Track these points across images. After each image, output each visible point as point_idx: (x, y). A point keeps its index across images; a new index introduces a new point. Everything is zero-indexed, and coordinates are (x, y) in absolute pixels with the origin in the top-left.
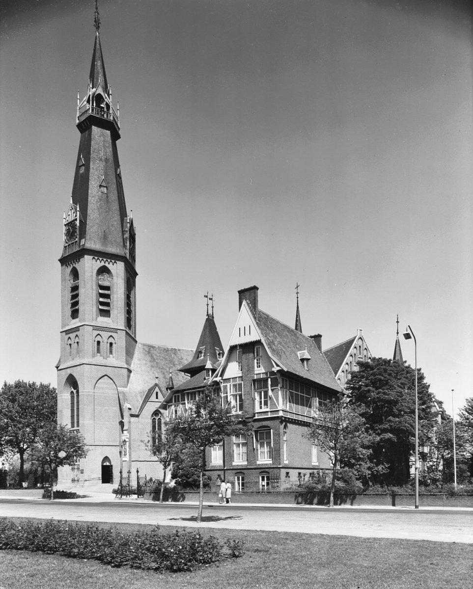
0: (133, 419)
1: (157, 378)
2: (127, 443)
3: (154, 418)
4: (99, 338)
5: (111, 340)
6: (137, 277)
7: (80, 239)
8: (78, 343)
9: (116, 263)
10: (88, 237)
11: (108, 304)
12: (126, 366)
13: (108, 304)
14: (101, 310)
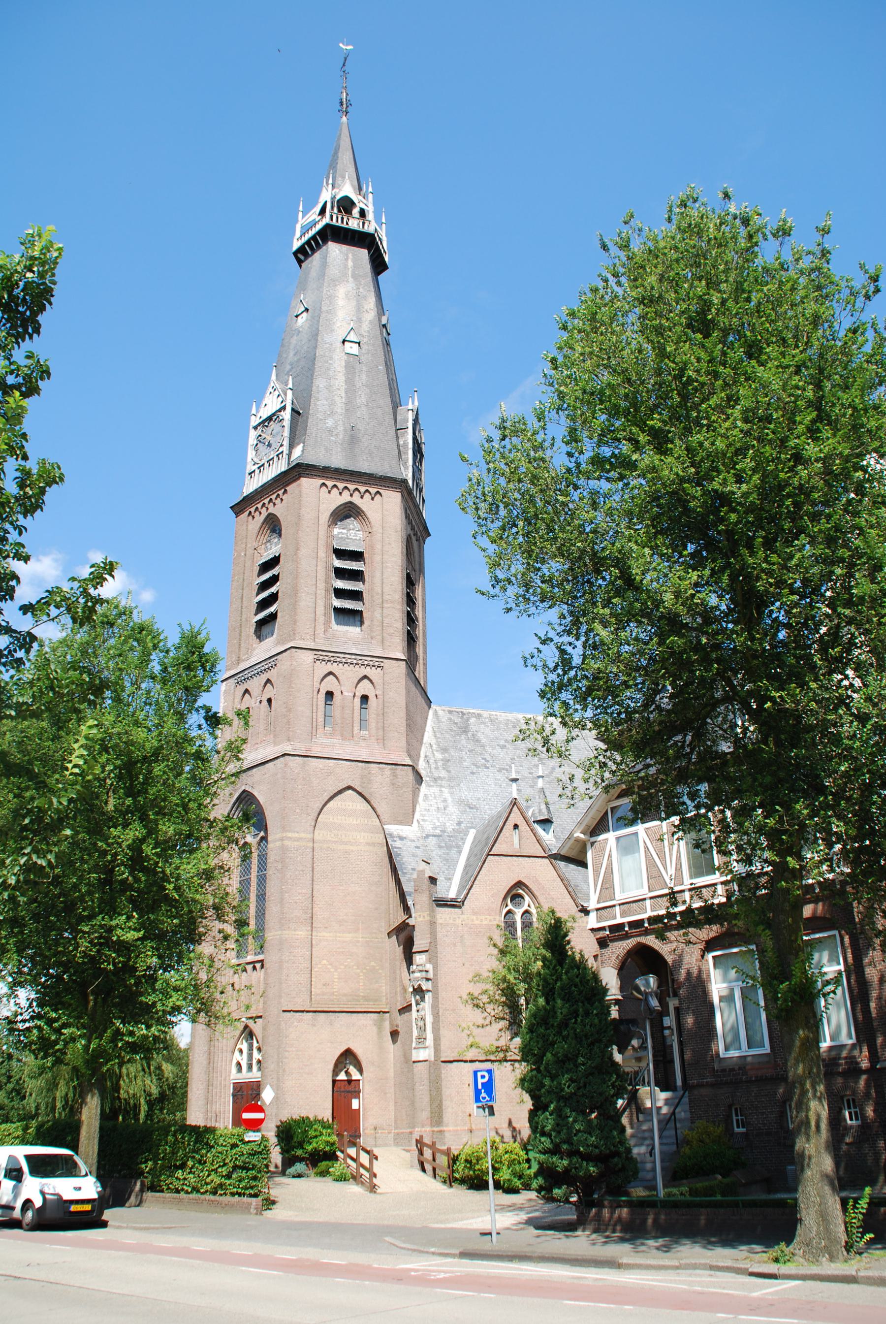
0: (444, 914)
1: (515, 780)
2: (428, 997)
3: (509, 912)
4: (330, 684)
5: (365, 688)
6: (428, 540)
7: (291, 446)
8: (269, 701)
9: (381, 495)
10: (310, 441)
11: (356, 596)
12: (408, 761)
13: (356, 596)
14: (338, 611)
